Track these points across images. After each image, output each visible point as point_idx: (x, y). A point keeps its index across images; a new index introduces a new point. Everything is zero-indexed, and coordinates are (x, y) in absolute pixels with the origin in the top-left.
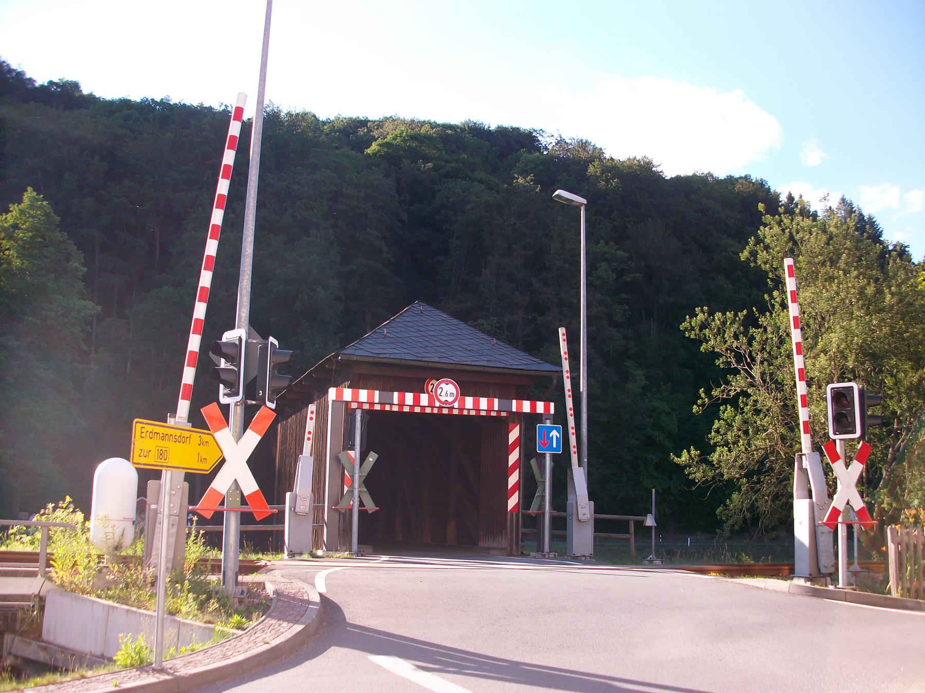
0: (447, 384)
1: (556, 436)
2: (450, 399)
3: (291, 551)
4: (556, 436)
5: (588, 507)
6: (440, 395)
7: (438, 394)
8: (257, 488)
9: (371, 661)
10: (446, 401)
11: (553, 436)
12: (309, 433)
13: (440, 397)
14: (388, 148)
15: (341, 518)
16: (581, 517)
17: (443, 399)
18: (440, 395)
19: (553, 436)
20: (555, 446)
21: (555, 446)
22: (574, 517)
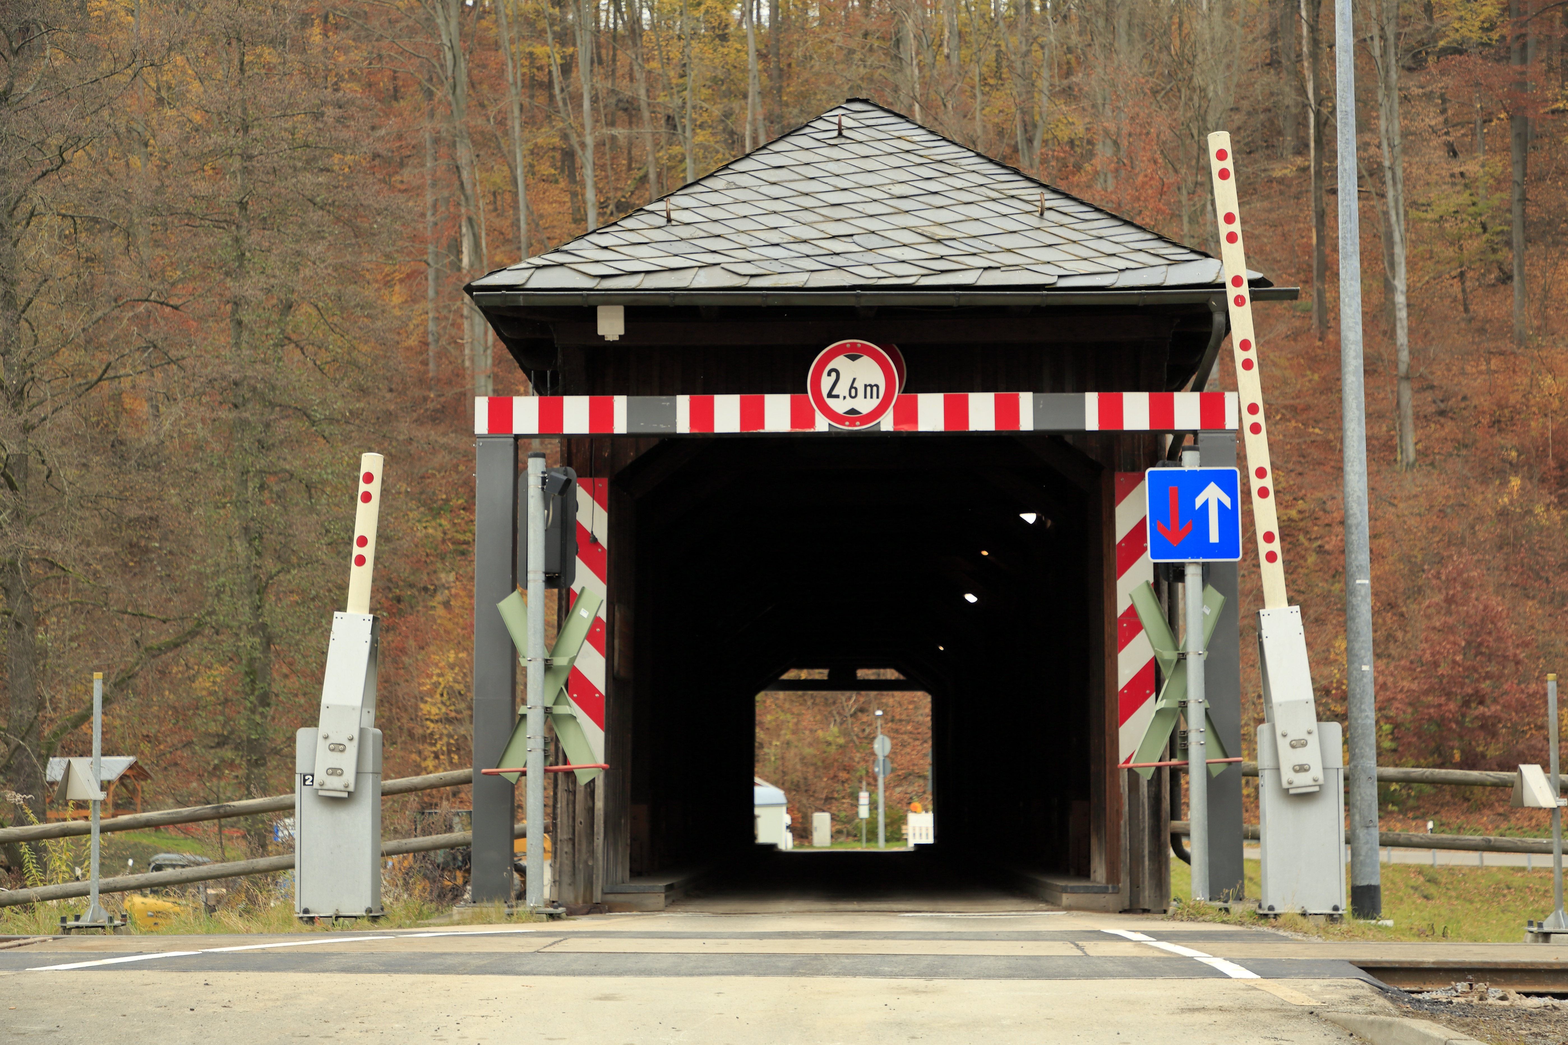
0: (853, 358)
1: (1220, 504)
2: (865, 406)
3: (306, 911)
4: (1220, 504)
5: (1313, 742)
6: (830, 395)
7: (825, 391)
8: (737, 398)
9: (129, 755)
10: (853, 411)
11: (1206, 504)
12: (361, 560)
13: (831, 402)
14: (164, 690)
15: (562, 796)
16: (1287, 775)
17: (839, 406)
18: (830, 395)
19: (1206, 504)
20: (1214, 537)
21: (1214, 537)
22: (1266, 782)
